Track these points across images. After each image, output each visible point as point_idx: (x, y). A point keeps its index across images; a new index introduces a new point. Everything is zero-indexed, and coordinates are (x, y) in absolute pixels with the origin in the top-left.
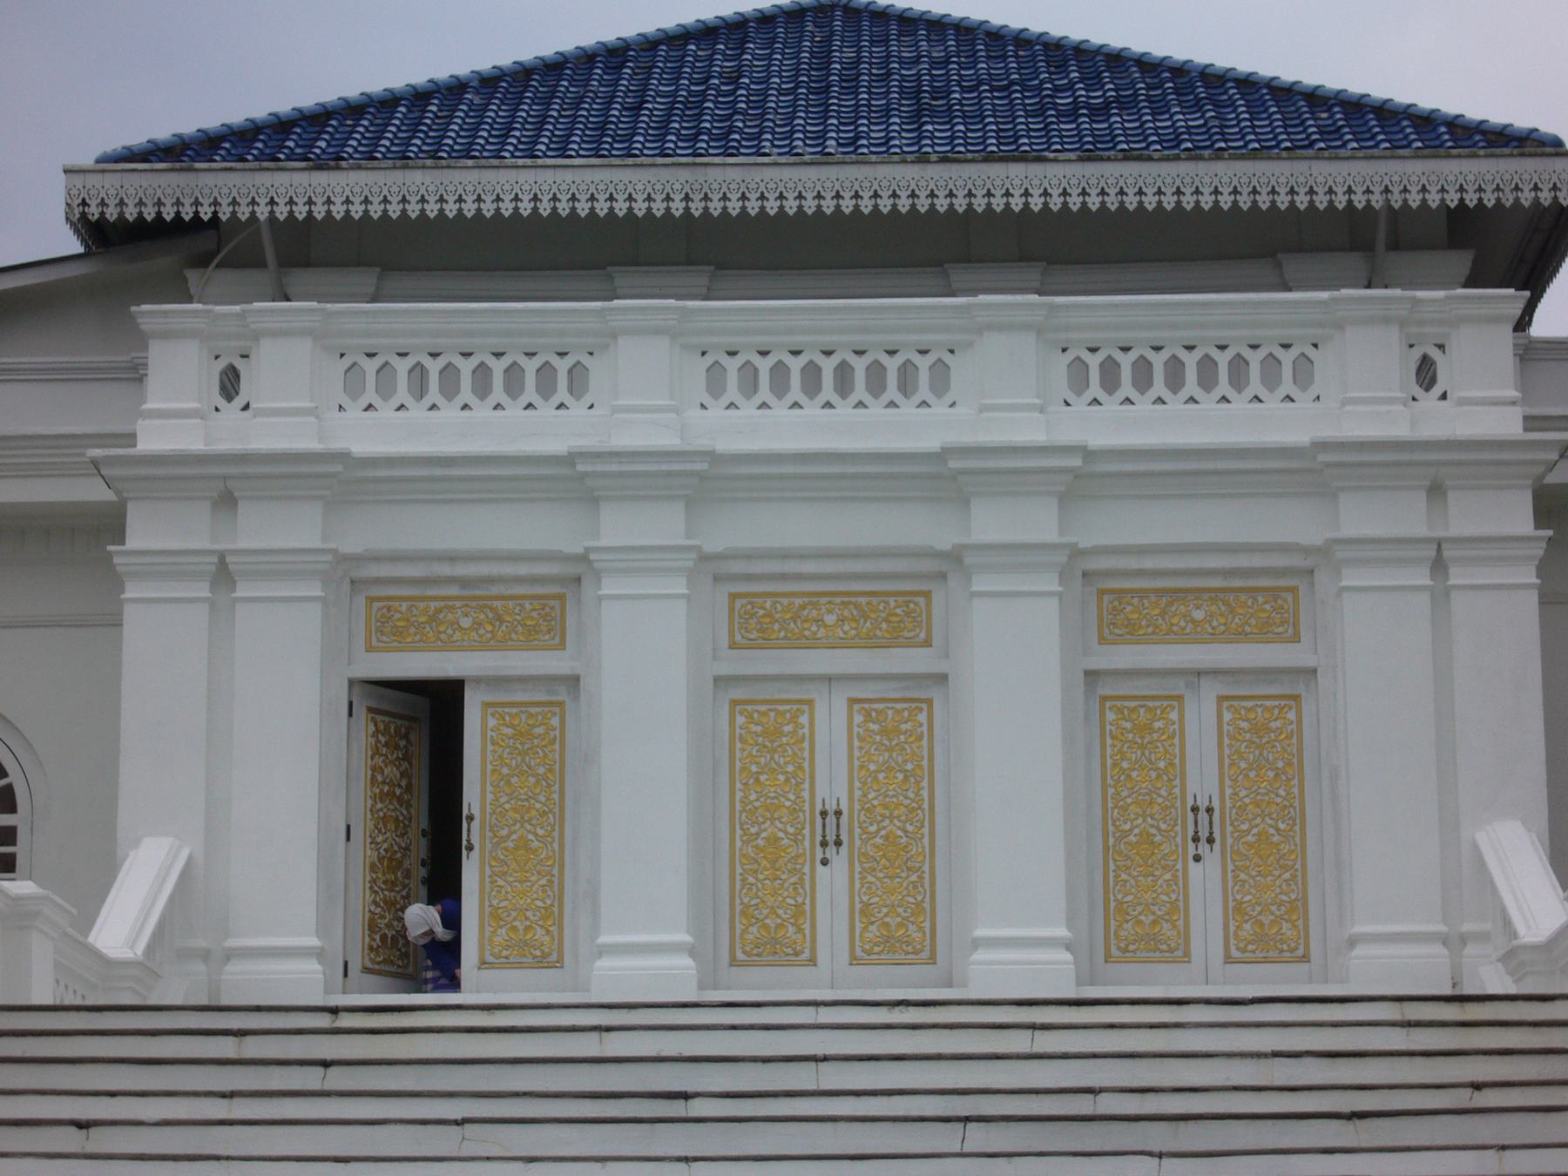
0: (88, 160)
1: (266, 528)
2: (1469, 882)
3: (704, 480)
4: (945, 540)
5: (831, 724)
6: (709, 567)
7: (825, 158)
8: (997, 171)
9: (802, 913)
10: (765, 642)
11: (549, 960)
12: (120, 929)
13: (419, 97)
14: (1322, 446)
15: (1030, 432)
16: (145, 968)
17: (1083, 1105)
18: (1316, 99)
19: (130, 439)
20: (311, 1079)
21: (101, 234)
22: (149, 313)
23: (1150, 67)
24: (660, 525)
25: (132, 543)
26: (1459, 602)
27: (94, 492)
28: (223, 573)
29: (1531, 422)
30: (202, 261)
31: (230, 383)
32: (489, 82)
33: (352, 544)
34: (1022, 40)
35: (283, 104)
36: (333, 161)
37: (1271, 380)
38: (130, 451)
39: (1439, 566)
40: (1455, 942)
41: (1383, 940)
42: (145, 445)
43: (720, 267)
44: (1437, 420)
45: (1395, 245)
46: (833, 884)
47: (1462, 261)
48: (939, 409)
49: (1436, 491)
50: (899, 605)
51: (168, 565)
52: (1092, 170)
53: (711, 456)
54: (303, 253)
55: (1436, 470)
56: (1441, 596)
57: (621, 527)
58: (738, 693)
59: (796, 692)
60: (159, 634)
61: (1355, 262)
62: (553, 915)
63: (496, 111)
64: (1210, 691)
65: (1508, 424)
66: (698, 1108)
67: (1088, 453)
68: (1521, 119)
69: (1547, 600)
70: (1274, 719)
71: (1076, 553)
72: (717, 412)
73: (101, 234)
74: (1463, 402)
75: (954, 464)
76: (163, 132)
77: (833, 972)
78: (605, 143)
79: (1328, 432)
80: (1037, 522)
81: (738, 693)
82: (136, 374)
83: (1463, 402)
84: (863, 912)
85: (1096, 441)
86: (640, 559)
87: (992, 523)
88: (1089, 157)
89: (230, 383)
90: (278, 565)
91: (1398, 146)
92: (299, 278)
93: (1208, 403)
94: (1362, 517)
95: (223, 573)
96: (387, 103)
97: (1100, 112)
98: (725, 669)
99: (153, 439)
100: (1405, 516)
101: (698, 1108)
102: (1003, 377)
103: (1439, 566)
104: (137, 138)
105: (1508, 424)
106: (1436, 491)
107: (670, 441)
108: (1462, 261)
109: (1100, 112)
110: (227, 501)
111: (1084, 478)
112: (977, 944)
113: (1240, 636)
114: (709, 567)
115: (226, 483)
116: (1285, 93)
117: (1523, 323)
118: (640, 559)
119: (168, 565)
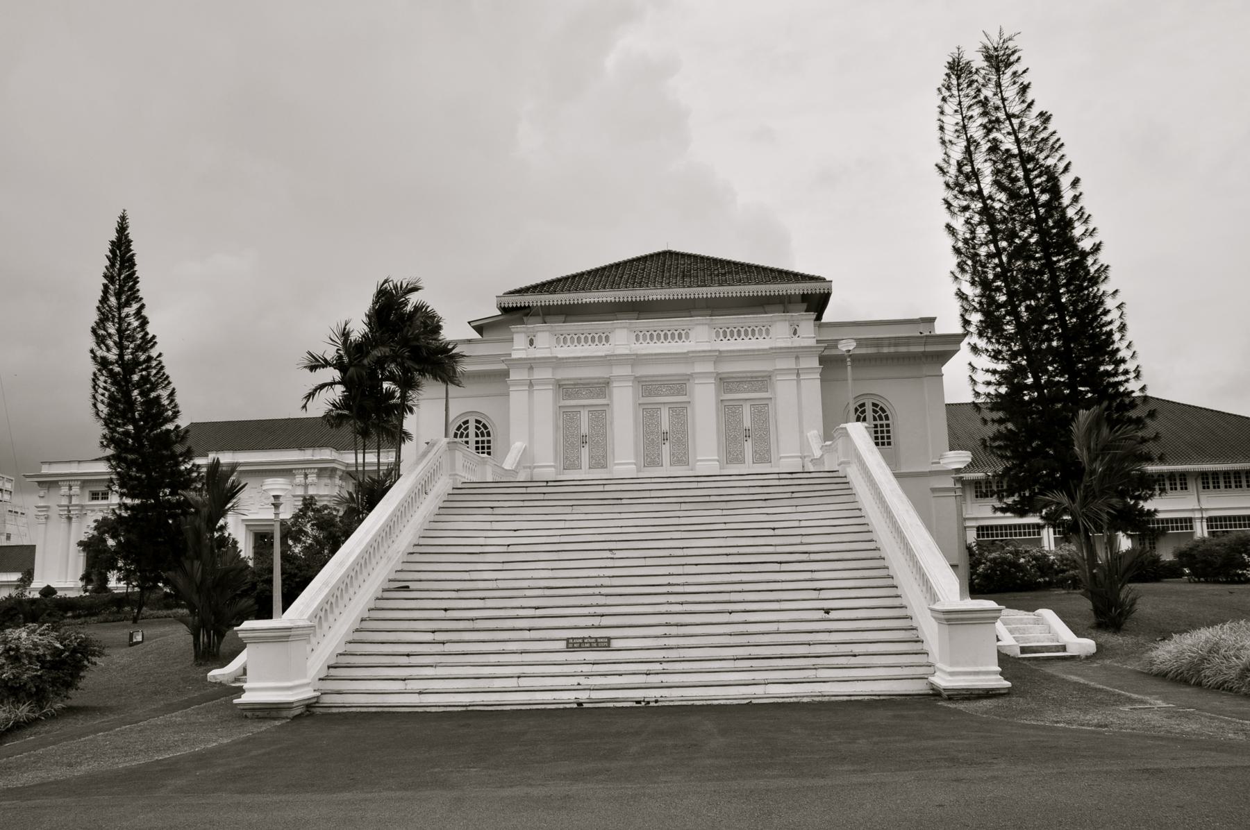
2: (804, 443)
3: (636, 360)
4: (770, 369)
5: (665, 414)
6: (637, 380)
7: (662, 287)
8: (700, 289)
9: (579, 458)
10: (650, 395)
11: (604, 467)
12: (509, 464)
13: (574, 277)
15: (706, 347)
16: (515, 472)
17: (707, 499)
18: (772, 270)
20: (541, 497)
21: (505, 310)
22: (514, 328)
23: (735, 264)
24: (626, 371)
28: (531, 384)
29: (818, 341)
30: (527, 315)
31: (531, 343)
32: (589, 273)
33: (558, 377)
34: (708, 259)
35: (554, 277)
36: (554, 292)
37: (760, 334)
38: (834, 352)
39: (798, 374)
40: (803, 458)
41: (786, 459)
42: (514, 356)
44: (797, 342)
45: (790, 302)
46: (666, 449)
47: (805, 306)
48: (687, 343)
49: (797, 358)
50: (680, 385)
51: (519, 383)
52: (721, 288)
53: (637, 355)
54: (548, 313)
55: (797, 353)
56: (798, 381)
57: (617, 371)
60: (518, 398)
61: (781, 307)
62: (605, 457)
63: (590, 279)
64: (586, 410)
65: (812, 342)
66: (624, 501)
68: (817, 274)
69: (822, 380)
70: (762, 411)
71: (718, 374)
72: (638, 345)
73: (505, 310)
76: (517, 288)
77: (667, 470)
78: (614, 285)
79: (773, 345)
80: (709, 367)
82: (511, 340)
84: (672, 455)
86: (622, 378)
87: (699, 368)
88: (721, 285)
89: (531, 343)
90: (543, 382)
91: (789, 281)
92: (547, 318)
93: (739, 340)
94: (781, 364)
95: (531, 384)
96: (567, 278)
97: (724, 275)
99: (515, 355)
100: (790, 364)
101: (624, 501)
102: (700, 336)
103: (798, 374)
104: (512, 289)
105: (812, 342)
106: (797, 358)
107: (627, 352)
108: (805, 306)
109: (724, 275)
110: (531, 368)
111: (719, 357)
113: (755, 391)
114: (637, 380)
115: (530, 364)
116: (765, 269)
117: (819, 318)
118: (622, 378)
119: (519, 383)
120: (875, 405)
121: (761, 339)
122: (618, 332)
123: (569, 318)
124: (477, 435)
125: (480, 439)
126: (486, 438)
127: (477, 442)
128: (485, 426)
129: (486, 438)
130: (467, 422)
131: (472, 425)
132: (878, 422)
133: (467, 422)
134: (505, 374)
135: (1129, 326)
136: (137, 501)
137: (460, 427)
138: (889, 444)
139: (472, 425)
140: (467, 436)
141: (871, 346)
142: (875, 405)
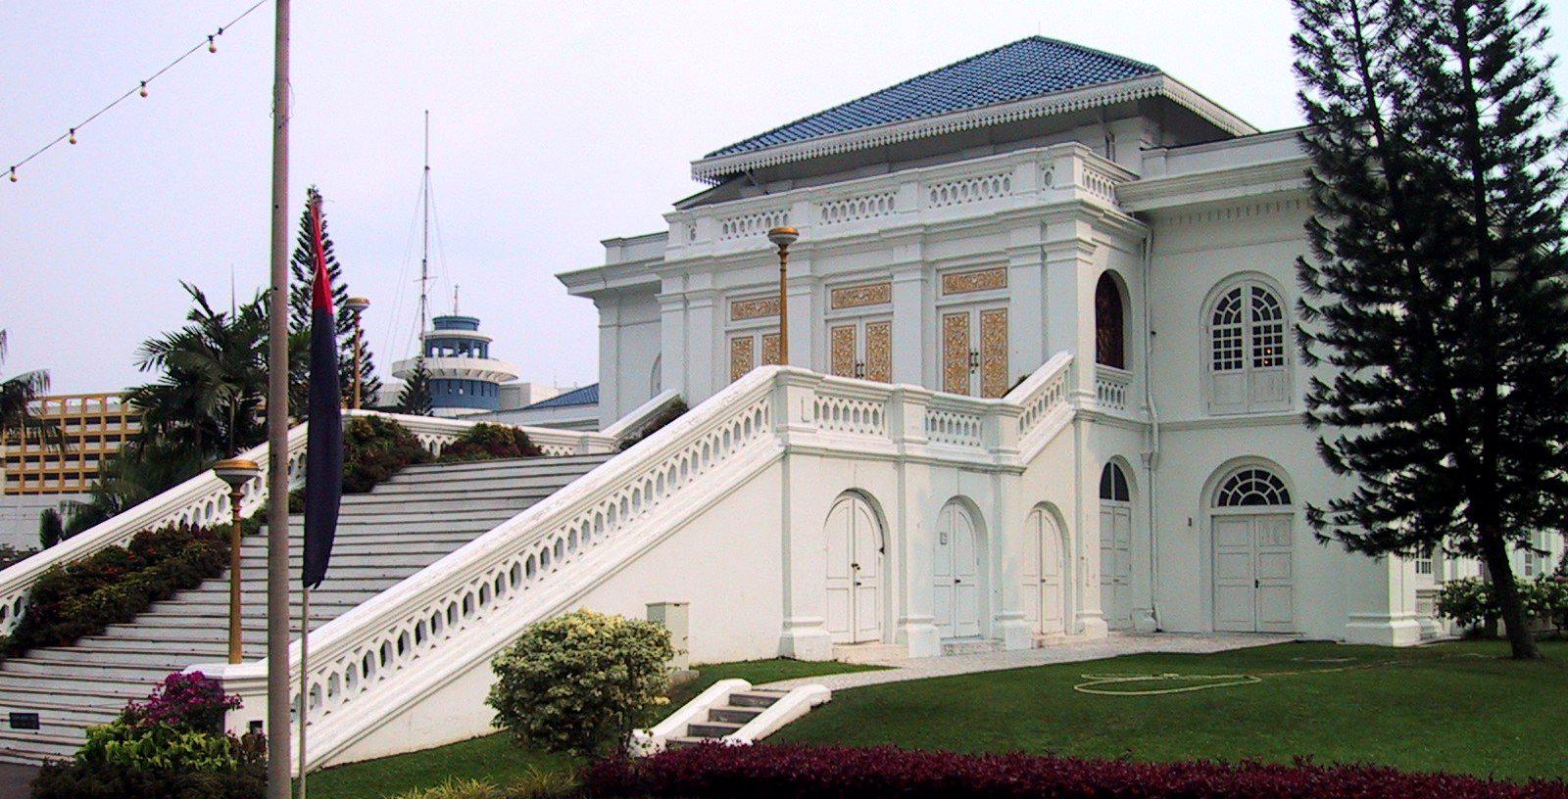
0: (701, 158)
1: (701, 282)
3: (927, 235)
6: (926, 266)
14: (998, 214)
19: (663, 258)
25: (664, 292)
26: (691, 313)
27: (655, 278)
39: (1044, 255)
42: (667, 260)
43: (997, 144)
50: (879, 291)
51: (672, 299)
56: (686, 310)
58: (734, 336)
59: (746, 334)
67: (926, 227)
74: (1060, 189)
75: (884, 236)
80: (914, 254)
81: (734, 336)
83: (1060, 189)
85: (928, 222)
90: (701, 294)
98: (829, 317)
100: (1029, 236)
103: (1044, 255)
112: (242, 558)
114: (926, 266)
115: (685, 268)
119: (672, 299)
120: (1257, 291)
121: (997, 198)
122: (1020, 169)
123: (799, 183)
124: (1256, 318)
125: (1262, 323)
126: (1273, 322)
127: (1257, 330)
128: (1271, 300)
129: (1273, 322)
130: (1236, 293)
131: (1246, 299)
132: (1262, 323)
133: (1236, 293)
134: (656, 287)
135: (428, 296)
136: (1376, 406)
137: (1225, 302)
138: (1217, 366)
139: (1246, 299)
140: (1238, 320)
141: (1263, 180)
142: (1257, 291)
